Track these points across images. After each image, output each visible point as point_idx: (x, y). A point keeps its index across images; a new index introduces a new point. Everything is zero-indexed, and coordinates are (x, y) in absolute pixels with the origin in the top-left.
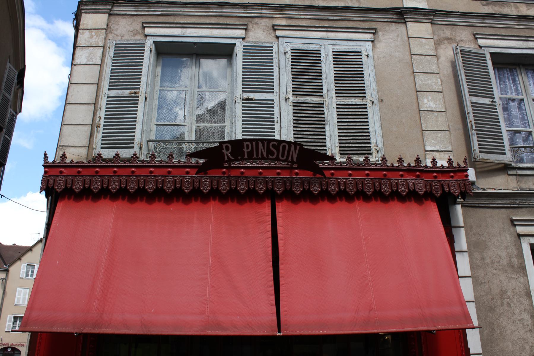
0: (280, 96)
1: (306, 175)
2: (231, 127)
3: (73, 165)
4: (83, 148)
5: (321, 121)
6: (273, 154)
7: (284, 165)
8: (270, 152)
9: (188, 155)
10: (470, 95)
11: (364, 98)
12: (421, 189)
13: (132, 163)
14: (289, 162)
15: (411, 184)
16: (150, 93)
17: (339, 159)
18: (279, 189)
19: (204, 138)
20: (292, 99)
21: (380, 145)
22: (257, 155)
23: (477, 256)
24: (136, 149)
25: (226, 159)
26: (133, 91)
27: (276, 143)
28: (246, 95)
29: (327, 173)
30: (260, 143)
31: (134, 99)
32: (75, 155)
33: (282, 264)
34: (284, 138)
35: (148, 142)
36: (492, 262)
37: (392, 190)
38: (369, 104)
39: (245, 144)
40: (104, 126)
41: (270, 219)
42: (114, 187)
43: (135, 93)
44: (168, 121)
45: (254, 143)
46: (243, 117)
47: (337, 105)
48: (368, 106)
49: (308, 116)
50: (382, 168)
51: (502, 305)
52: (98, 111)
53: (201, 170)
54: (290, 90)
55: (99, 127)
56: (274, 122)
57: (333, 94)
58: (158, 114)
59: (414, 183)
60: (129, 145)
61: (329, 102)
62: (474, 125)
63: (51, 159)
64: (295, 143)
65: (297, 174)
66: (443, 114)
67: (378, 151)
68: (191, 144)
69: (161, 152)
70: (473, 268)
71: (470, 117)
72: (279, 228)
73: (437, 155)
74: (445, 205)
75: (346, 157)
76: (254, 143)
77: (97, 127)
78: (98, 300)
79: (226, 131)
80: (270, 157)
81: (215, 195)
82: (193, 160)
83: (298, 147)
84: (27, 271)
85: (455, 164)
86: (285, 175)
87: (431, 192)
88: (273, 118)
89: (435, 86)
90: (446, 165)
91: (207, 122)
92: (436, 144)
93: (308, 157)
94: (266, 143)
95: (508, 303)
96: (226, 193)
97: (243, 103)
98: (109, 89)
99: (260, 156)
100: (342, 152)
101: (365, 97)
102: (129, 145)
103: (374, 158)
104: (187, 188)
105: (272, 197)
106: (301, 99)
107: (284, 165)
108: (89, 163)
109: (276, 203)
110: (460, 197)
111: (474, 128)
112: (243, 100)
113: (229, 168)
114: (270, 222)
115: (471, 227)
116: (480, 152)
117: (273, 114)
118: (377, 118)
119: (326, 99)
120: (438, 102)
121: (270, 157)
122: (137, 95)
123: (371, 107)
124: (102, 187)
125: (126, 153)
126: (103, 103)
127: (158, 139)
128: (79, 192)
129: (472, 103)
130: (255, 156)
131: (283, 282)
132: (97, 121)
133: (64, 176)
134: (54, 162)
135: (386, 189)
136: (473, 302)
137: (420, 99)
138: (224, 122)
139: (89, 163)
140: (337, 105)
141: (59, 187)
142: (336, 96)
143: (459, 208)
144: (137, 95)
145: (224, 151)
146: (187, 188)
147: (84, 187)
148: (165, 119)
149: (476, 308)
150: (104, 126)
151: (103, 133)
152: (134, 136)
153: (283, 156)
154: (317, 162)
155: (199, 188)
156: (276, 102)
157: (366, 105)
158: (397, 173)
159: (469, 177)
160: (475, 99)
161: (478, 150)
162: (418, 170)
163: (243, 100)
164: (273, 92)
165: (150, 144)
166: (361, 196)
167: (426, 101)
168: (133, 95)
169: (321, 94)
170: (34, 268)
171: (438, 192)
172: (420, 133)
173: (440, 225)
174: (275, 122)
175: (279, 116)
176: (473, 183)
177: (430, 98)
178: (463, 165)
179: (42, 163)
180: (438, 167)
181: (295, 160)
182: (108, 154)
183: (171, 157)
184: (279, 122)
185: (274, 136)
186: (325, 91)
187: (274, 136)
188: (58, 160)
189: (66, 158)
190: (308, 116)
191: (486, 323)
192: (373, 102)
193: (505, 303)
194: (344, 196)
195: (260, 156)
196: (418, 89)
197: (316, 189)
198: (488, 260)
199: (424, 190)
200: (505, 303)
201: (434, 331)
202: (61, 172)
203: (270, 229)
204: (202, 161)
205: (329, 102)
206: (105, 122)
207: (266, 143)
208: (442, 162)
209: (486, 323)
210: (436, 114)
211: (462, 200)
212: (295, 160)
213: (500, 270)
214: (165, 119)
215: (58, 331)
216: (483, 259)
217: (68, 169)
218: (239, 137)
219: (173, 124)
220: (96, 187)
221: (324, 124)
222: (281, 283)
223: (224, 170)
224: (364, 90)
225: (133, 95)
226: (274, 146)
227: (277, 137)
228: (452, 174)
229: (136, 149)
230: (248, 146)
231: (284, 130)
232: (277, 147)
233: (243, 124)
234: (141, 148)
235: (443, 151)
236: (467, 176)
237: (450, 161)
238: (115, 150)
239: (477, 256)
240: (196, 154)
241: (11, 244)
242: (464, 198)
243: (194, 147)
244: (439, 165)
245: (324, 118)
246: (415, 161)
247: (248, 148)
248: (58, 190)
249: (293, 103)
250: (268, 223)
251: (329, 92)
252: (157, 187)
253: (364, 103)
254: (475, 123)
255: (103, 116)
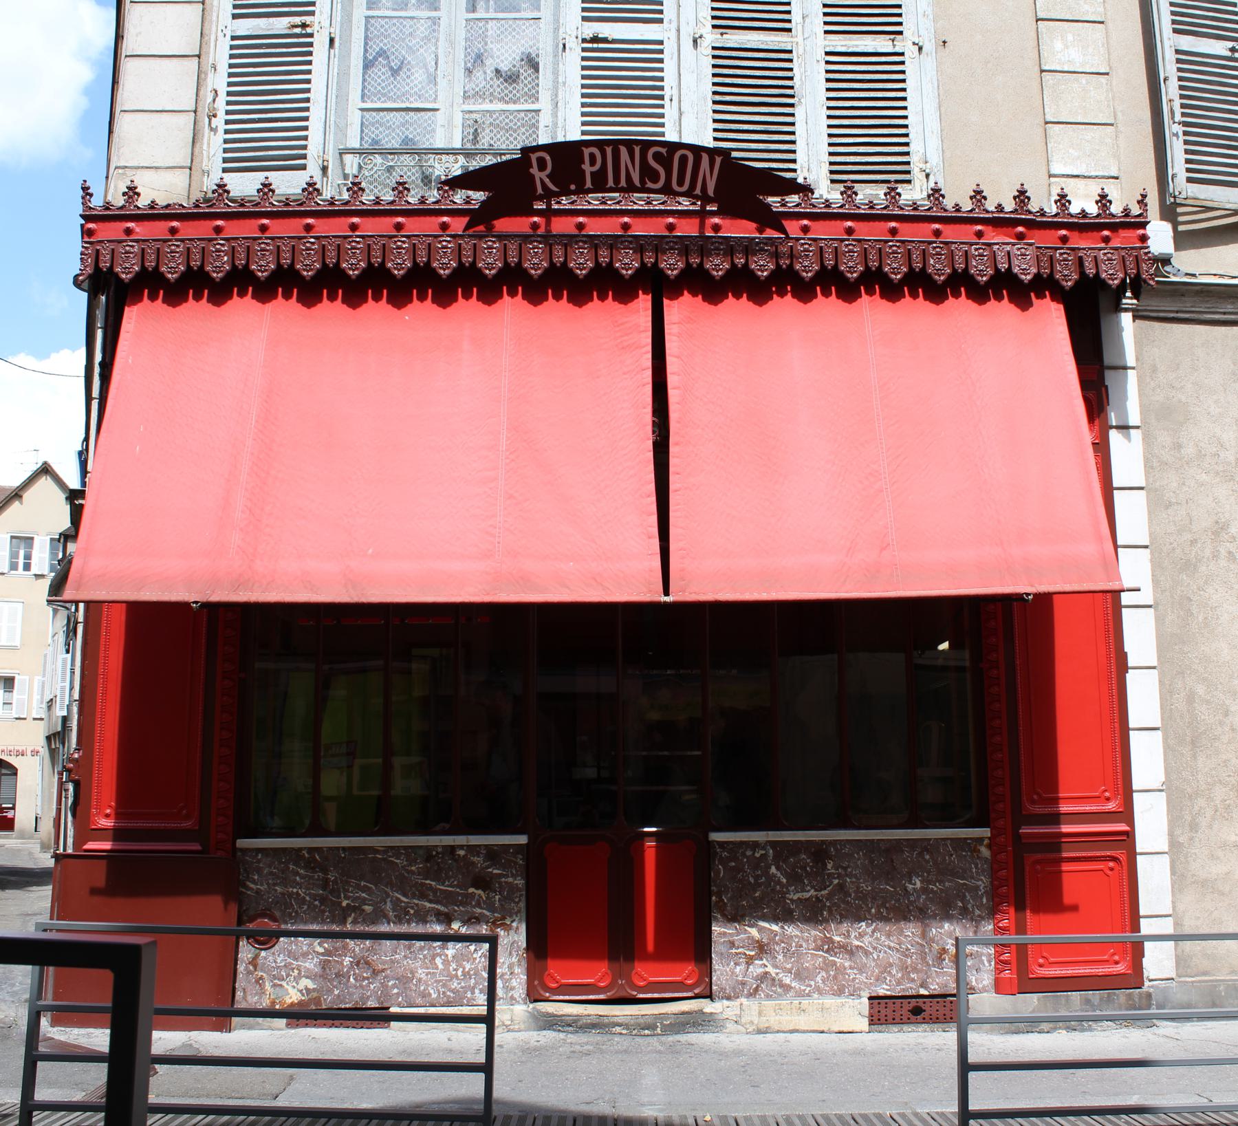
0: (678, 31)
1: (740, 230)
2: (555, 115)
3: (154, 215)
4: (178, 172)
5: (783, 96)
6: (655, 179)
7: (685, 204)
8: (648, 173)
9: (446, 183)
10: (1175, 31)
11: (898, 37)
12: (1025, 269)
13: (302, 210)
14: (697, 197)
15: (1001, 256)
16: (342, 24)
17: (826, 192)
18: (672, 265)
19: (484, 142)
20: (711, 37)
21: (935, 160)
22: (617, 179)
23: (1164, 438)
24: (313, 170)
25: (540, 191)
26: (297, 20)
27: (663, 151)
28: (591, 29)
29: (793, 227)
30: (623, 151)
31: (299, 45)
32: (163, 188)
33: (677, 444)
34: (688, 139)
35: (341, 154)
36: (1200, 455)
37: (954, 270)
38: (910, 51)
39: (587, 152)
40: (228, 113)
41: (650, 340)
42: (263, 267)
43: (304, 26)
44: (390, 99)
45: (609, 150)
46: (583, 86)
47: (827, 54)
48: (906, 58)
49: (754, 83)
50: (936, 215)
51: (1215, 556)
52: (211, 75)
53: (480, 218)
54: (706, 14)
55: (215, 116)
56: (662, 98)
57: (817, 23)
58: (364, 80)
59: (1009, 253)
60: (295, 161)
61: (805, 46)
62: (1178, 111)
63: (97, 202)
64: (712, 152)
65: (716, 228)
66: (1103, 79)
67: (927, 176)
68: (451, 158)
69: (376, 180)
70: (1152, 467)
71: (1170, 90)
72: (669, 359)
73: (1071, 187)
74: (1088, 313)
75: (841, 187)
76: (609, 150)
77: (209, 117)
78: (241, 530)
79: (541, 125)
80: (650, 185)
81: (512, 281)
82: (459, 197)
83: (718, 160)
84: (14, 555)
85: (1116, 209)
86: (687, 229)
87: (1051, 275)
88: (662, 88)
89: (1086, 7)
90: (1093, 209)
91: (491, 101)
92: (1078, 158)
93: (746, 186)
94: (637, 149)
95: (1230, 553)
96: (541, 276)
97: (584, 50)
98: (235, 17)
99: (623, 183)
100: (836, 174)
101: (901, 33)
102: (295, 161)
103: (914, 194)
104: (445, 265)
105: (659, 287)
106: (735, 39)
107: (685, 204)
108: (197, 206)
109: (666, 302)
110: (1128, 294)
111: (1178, 118)
112: (584, 41)
113: (548, 214)
114: (649, 348)
115: (1154, 369)
116: (1189, 180)
117: (662, 79)
118: (930, 90)
119: (800, 39)
120: (1090, 50)
121: (650, 185)
122: (309, 30)
123: (917, 60)
124: (234, 267)
125: (288, 184)
126: (220, 54)
127: (366, 146)
128: (177, 280)
129: (1177, 52)
130: (611, 183)
131: (678, 485)
132: (210, 99)
133: (137, 241)
134: (107, 206)
135: (939, 269)
136: (1146, 547)
137: (1044, 38)
138: (537, 99)
139: (197, 206)
140: (827, 54)
141: (127, 269)
142: (826, 32)
143: (1126, 318)
144: (309, 30)
145: (534, 171)
146: (445, 265)
147: (189, 267)
148: (384, 95)
149: (1151, 561)
150: (228, 113)
151: (227, 132)
152: (306, 138)
153: (680, 184)
154: (770, 199)
155: (474, 264)
156: (669, 48)
157: (902, 54)
158: (968, 227)
159: (1150, 242)
160: (1187, 43)
161: (1182, 175)
162: (1020, 221)
163: (584, 41)
164: (661, 21)
165: (348, 158)
166: (877, 283)
167: (1058, 45)
168: (298, 30)
169: (787, 25)
170: (31, 546)
171: (1068, 278)
172: (1041, 130)
173: (1066, 357)
174: (667, 98)
175: (675, 84)
176: (1166, 260)
177: (1070, 37)
178: (1136, 210)
179: (80, 210)
180: (1071, 216)
181: (711, 193)
182: (244, 185)
183: (401, 188)
184: (675, 99)
185: (663, 134)
186: (796, 17)
187: (663, 134)
188: (120, 201)
189: (139, 195)
190: (754, 83)
191: (1172, 597)
192: (920, 49)
193: (1223, 552)
194: (834, 282)
195: (623, 183)
196: (1040, 15)
197: (762, 266)
198: (1189, 450)
199: (1034, 270)
200: (1223, 552)
201: (1028, 594)
202: (128, 232)
203: (649, 364)
204: (479, 196)
205: (805, 46)
206: (228, 103)
207: (637, 149)
208: (1083, 202)
209: (1172, 597)
210: (1083, 79)
211: (1135, 301)
212: (711, 193)
213: (1217, 473)
214: (384, 95)
215: (154, 599)
216: (1178, 446)
217: (146, 223)
218: (574, 135)
219: (403, 106)
220: (219, 267)
221: (792, 105)
222: (672, 487)
223: (536, 219)
224: (900, 15)
225: (298, 30)
226: (657, 156)
227: (671, 136)
228: (1106, 233)
229: (313, 170)
230: (592, 156)
231: (690, 119)
232: (665, 161)
233: (583, 105)
234: (324, 169)
235: (1096, 177)
236: (1144, 238)
237: (1103, 200)
238: (260, 177)
239: (1164, 438)
240: (467, 180)
241: (53, 355)
242: (1136, 295)
243: (460, 164)
244: (1074, 209)
245: (792, 88)
246: (1015, 198)
247: (593, 163)
248: (124, 276)
249: (714, 48)
250: (644, 350)
251: (807, 20)
252: (370, 264)
253: (898, 50)
254: (1183, 106)
255: (223, 89)
